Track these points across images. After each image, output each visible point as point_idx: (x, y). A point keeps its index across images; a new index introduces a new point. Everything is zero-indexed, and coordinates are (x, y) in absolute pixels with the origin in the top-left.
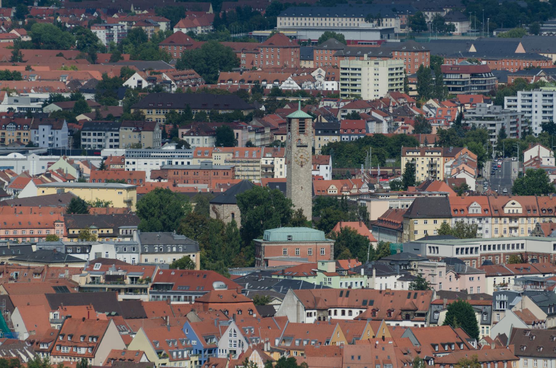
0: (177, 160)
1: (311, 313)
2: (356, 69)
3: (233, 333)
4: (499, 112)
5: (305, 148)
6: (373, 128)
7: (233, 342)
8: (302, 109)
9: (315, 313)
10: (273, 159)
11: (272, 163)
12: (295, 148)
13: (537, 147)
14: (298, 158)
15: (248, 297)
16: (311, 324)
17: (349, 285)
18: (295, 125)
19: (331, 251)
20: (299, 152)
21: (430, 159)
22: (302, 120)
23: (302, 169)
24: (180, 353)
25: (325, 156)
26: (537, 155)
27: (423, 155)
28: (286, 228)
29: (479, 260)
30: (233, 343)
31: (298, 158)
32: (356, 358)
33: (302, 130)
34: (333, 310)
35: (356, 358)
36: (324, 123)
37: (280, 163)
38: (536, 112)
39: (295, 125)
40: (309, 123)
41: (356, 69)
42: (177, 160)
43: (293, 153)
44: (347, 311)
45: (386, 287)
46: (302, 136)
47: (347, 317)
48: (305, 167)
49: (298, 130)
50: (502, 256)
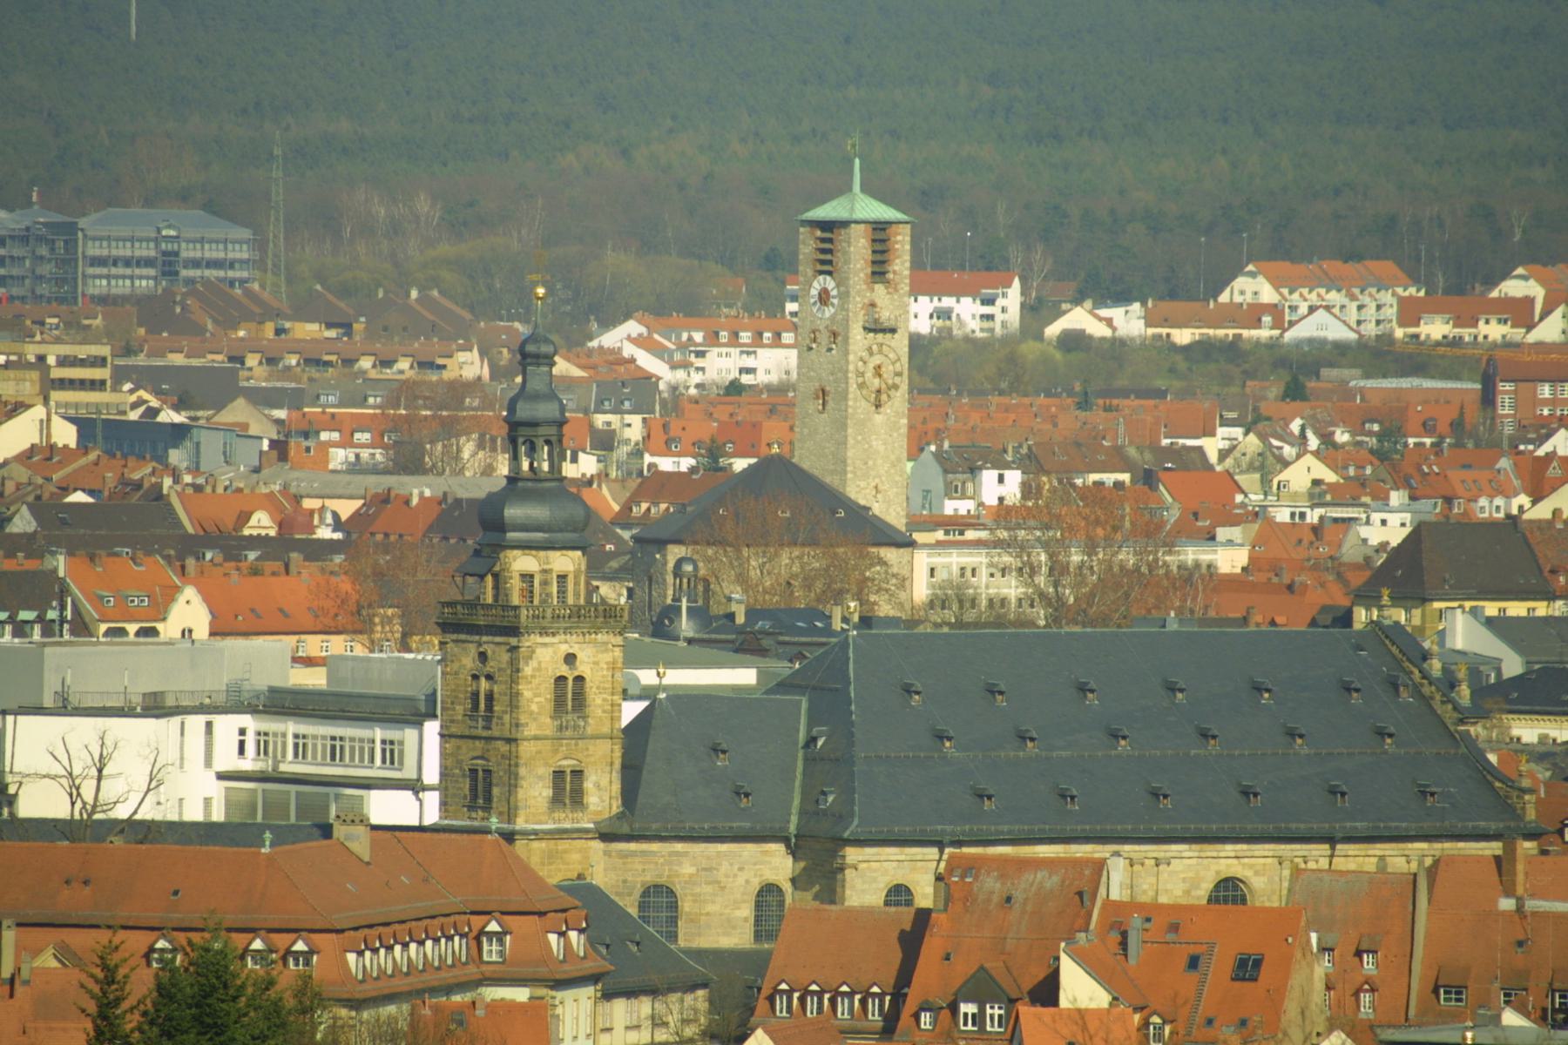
0: (41, 349)
2: (242, 744)
4: (720, 407)
5: (889, 336)
8: (867, 189)
12: (858, 338)
14: (869, 375)
18: (857, 247)
20: (871, 354)
22: (880, 229)
23: (878, 418)
24: (525, 465)
31: (869, 375)
33: (879, 271)
39: (857, 247)
41: (242, 744)
42: (41, 349)
43: (851, 357)
48: (887, 409)
49: (869, 270)
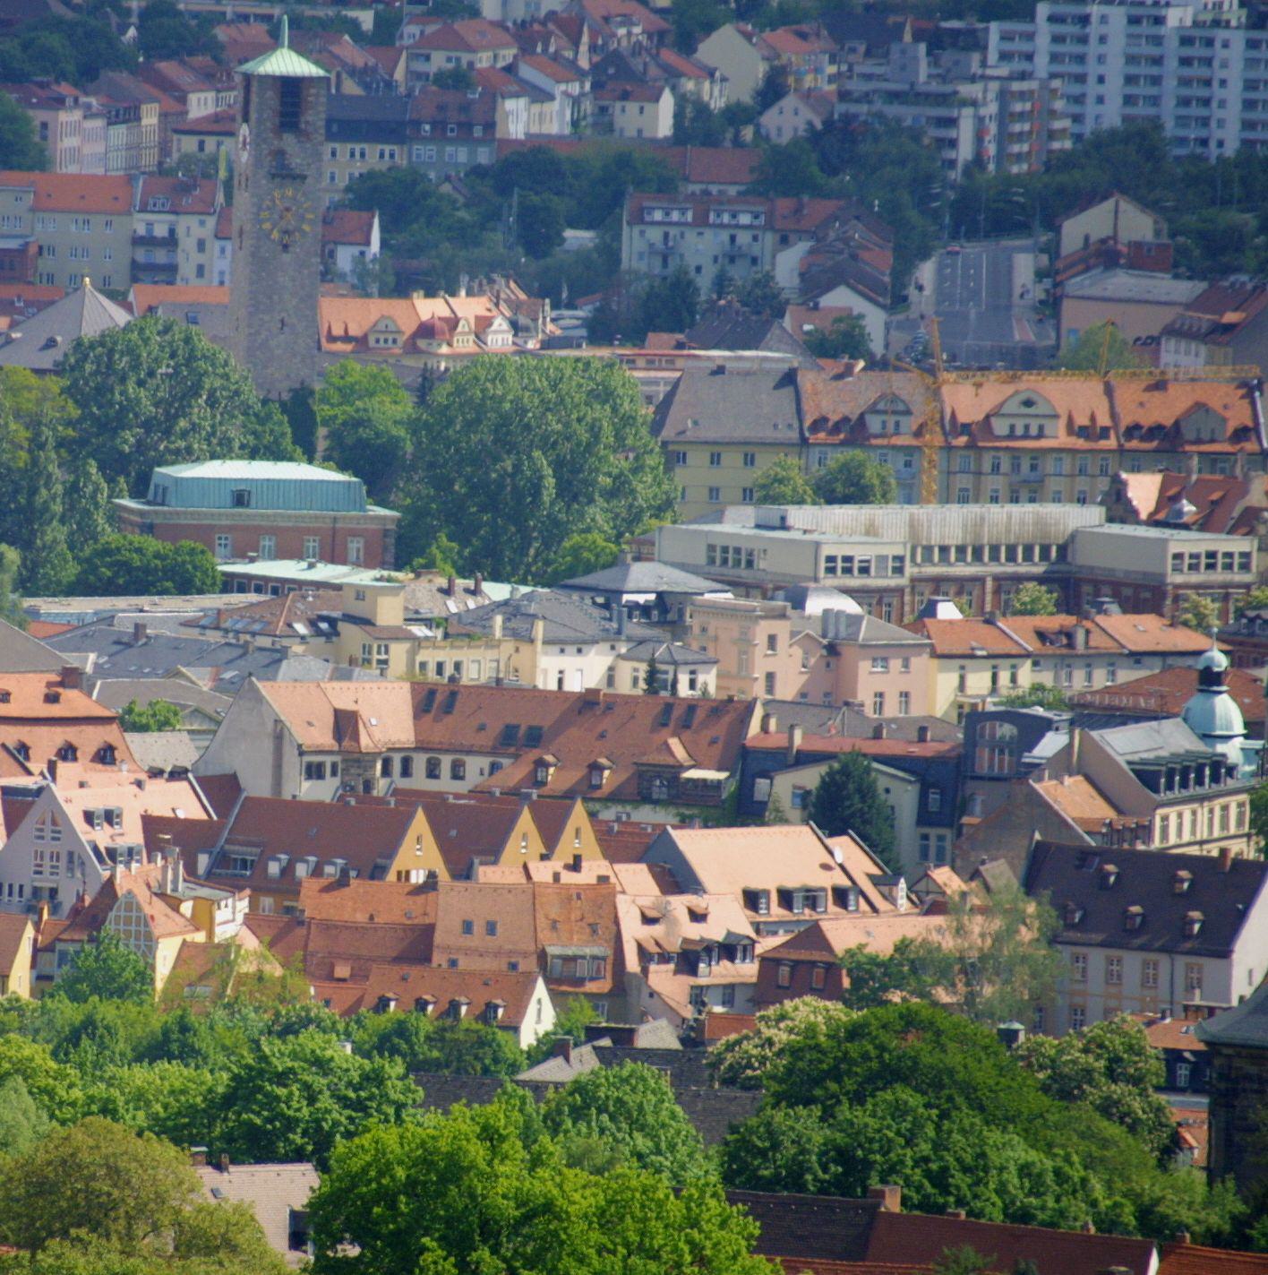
1: (320, 766)
3: (48, 827)
6: (519, 119)
7: (47, 858)
9: (334, 766)
10: (172, 217)
11: (172, 232)
13: (1109, 205)
15: (97, 702)
16: (651, 869)
17: (449, 670)
19: (385, 549)
21: (725, 236)
23: (286, 257)
25: (354, 217)
26: (1110, 232)
27: (701, 222)
28: (229, 463)
29: (907, 598)
30: (47, 862)
32: (479, 928)
34: (446, 761)
35: (479, 928)
36: (352, 98)
37: (198, 232)
38: (1101, 80)
40: (317, 95)
44: (446, 761)
45: (560, 681)
46: (289, 142)
47: (445, 784)
50: (989, 584)
